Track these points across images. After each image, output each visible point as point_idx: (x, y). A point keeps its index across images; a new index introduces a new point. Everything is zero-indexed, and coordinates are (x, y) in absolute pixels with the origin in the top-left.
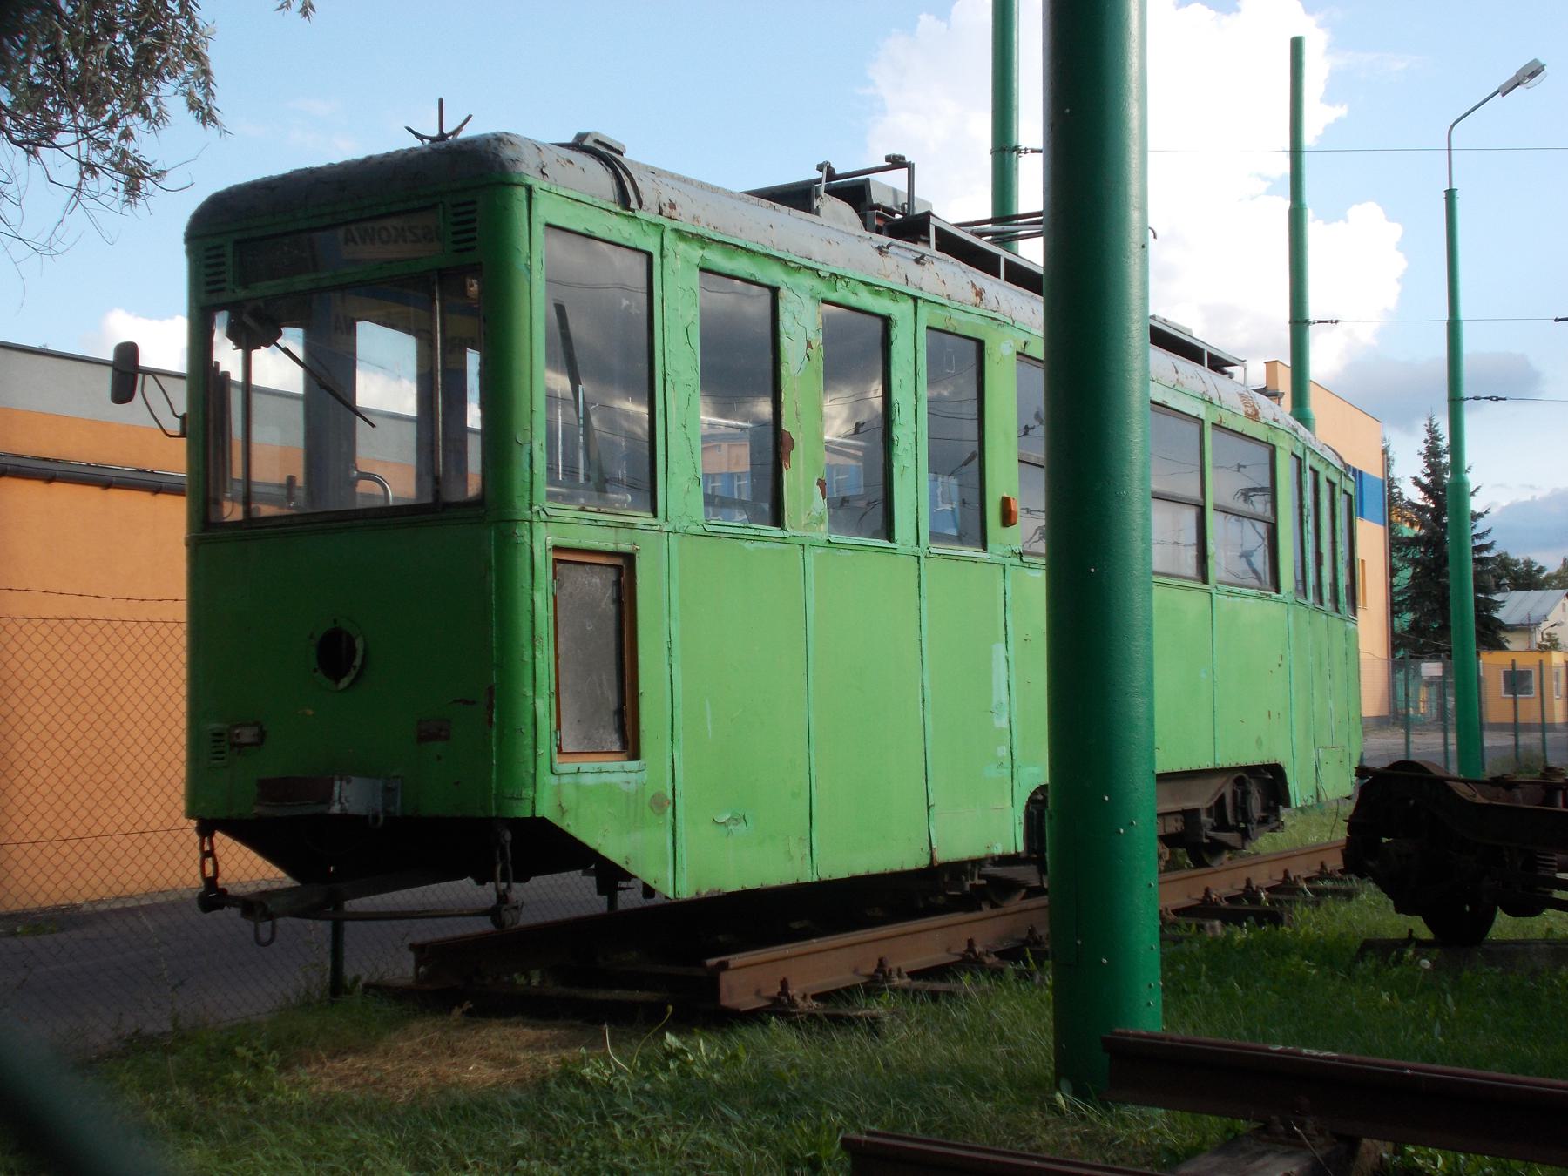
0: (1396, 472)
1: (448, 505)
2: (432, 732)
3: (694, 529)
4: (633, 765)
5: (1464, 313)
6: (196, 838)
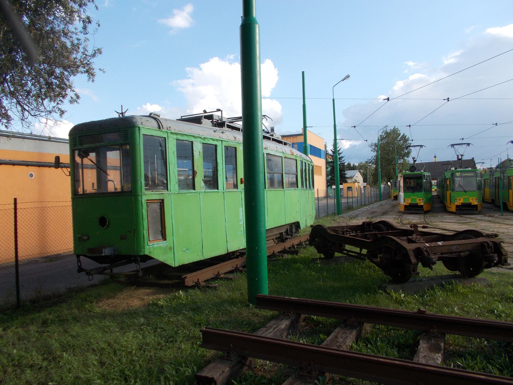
0: (327, 149)
1: (125, 192)
2: (123, 238)
3: (176, 192)
4: (165, 242)
5: (336, 123)
6: (76, 258)
